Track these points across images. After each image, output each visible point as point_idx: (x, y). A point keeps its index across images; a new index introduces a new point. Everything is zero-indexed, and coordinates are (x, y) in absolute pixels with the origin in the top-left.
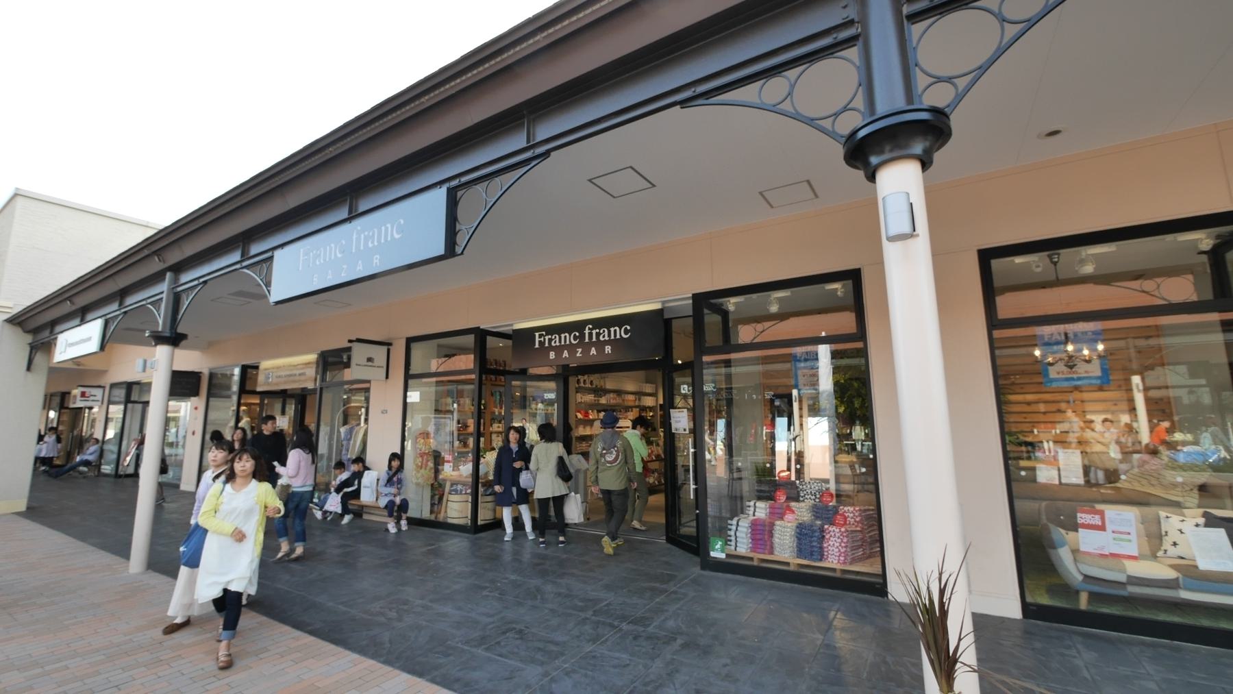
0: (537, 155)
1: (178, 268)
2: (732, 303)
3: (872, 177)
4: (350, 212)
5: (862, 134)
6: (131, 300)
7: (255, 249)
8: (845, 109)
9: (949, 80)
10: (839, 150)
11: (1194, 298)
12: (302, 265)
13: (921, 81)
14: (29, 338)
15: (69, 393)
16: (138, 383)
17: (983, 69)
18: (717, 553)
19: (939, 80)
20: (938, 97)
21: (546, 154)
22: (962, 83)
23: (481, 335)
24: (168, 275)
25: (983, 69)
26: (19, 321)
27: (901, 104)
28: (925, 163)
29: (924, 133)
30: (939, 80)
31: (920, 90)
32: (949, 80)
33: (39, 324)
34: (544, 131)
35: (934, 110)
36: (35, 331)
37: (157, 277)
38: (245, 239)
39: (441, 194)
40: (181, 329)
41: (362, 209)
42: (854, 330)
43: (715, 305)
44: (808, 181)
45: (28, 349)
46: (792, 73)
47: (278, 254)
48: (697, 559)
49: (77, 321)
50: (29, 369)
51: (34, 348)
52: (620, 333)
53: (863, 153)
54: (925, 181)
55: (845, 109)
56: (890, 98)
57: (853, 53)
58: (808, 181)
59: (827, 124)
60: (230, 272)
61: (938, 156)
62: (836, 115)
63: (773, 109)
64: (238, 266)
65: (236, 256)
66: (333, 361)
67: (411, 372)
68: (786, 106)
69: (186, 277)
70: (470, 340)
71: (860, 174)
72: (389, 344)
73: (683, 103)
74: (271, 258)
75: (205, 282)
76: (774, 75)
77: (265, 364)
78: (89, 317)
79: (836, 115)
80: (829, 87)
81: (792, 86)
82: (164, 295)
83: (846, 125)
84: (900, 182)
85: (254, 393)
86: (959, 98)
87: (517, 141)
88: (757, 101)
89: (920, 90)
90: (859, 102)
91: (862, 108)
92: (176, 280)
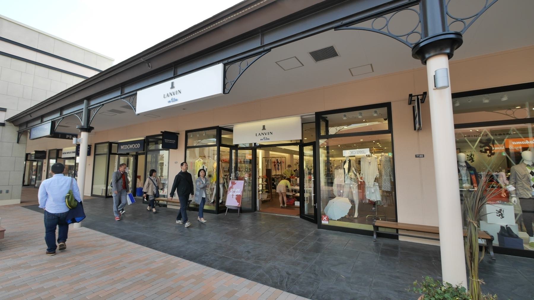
0: (265, 50)
1: (89, 99)
2: (329, 117)
3: (425, 63)
4: (174, 75)
5: (422, 45)
6: (65, 112)
7: (127, 90)
8: (412, 32)
9: (462, 20)
10: (410, 51)
11: (528, 117)
12: (151, 98)
13: (449, 20)
14: (17, 129)
15: (61, 150)
16: (30, 154)
17: (477, 15)
18: (324, 222)
19: (457, 20)
20: (454, 28)
21: (269, 50)
22: (467, 22)
23: (110, 144)
24: (85, 101)
25: (477, 15)
26: (13, 121)
27: (440, 31)
28: (450, 56)
29: (450, 44)
30: (457, 20)
31: (448, 25)
32: (462, 20)
33: (23, 123)
34: (269, 39)
35: (456, 34)
36: (20, 126)
37: (80, 102)
38: (122, 86)
39: (220, 66)
40: (91, 125)
41: (179, 73)
42: (305, 148)
43: (324, 117)
44: (371, 65)
45: (17, 133)
46: (388, 16)
47: (139, 93)
48: (317, 225)
49: (39, 121)
50: (18, 142)
51: (20, 133)
52: (138, 146)
53: (422, 53)
54: (449, 62)
55: (412, 32)
56: (435, 29)
57: (417, 7)
58: (371, 65)
59: (404, 39)
60: (116, 99)
61: (455, 52)
62: (408, 35)
63: (378, 32)
64: (120, 98)
65: (118, 93)
66: (318, 124)
67: (188, 145)
68: (385, 30)
69: (93, 103)
70: (214, 132)
71: (419, 61)
72: (179, 134)
73: (336, 28)
74: (136, 94)
75: (103, 105)
76: (379, 17)
77: (238, 128)
78: (45, 119)
79: (408, 35)
80: (405, 21)
81: (388, 22)
82: (84, 110)
83: (415, 39)
84: (438, 65)
85: (61, 158)
86: (466, 28)
87: (255, 44)
88: (370, 27)
89: (448, 25)
90: (419, 29)
91: (420, 32)
92: (88, 104)
